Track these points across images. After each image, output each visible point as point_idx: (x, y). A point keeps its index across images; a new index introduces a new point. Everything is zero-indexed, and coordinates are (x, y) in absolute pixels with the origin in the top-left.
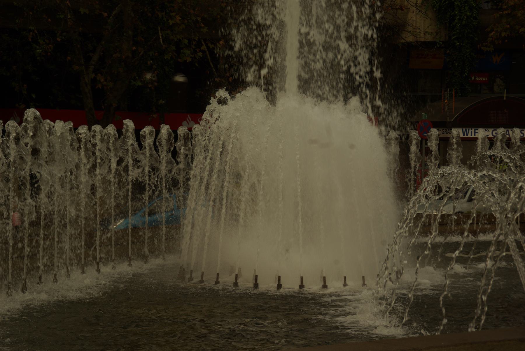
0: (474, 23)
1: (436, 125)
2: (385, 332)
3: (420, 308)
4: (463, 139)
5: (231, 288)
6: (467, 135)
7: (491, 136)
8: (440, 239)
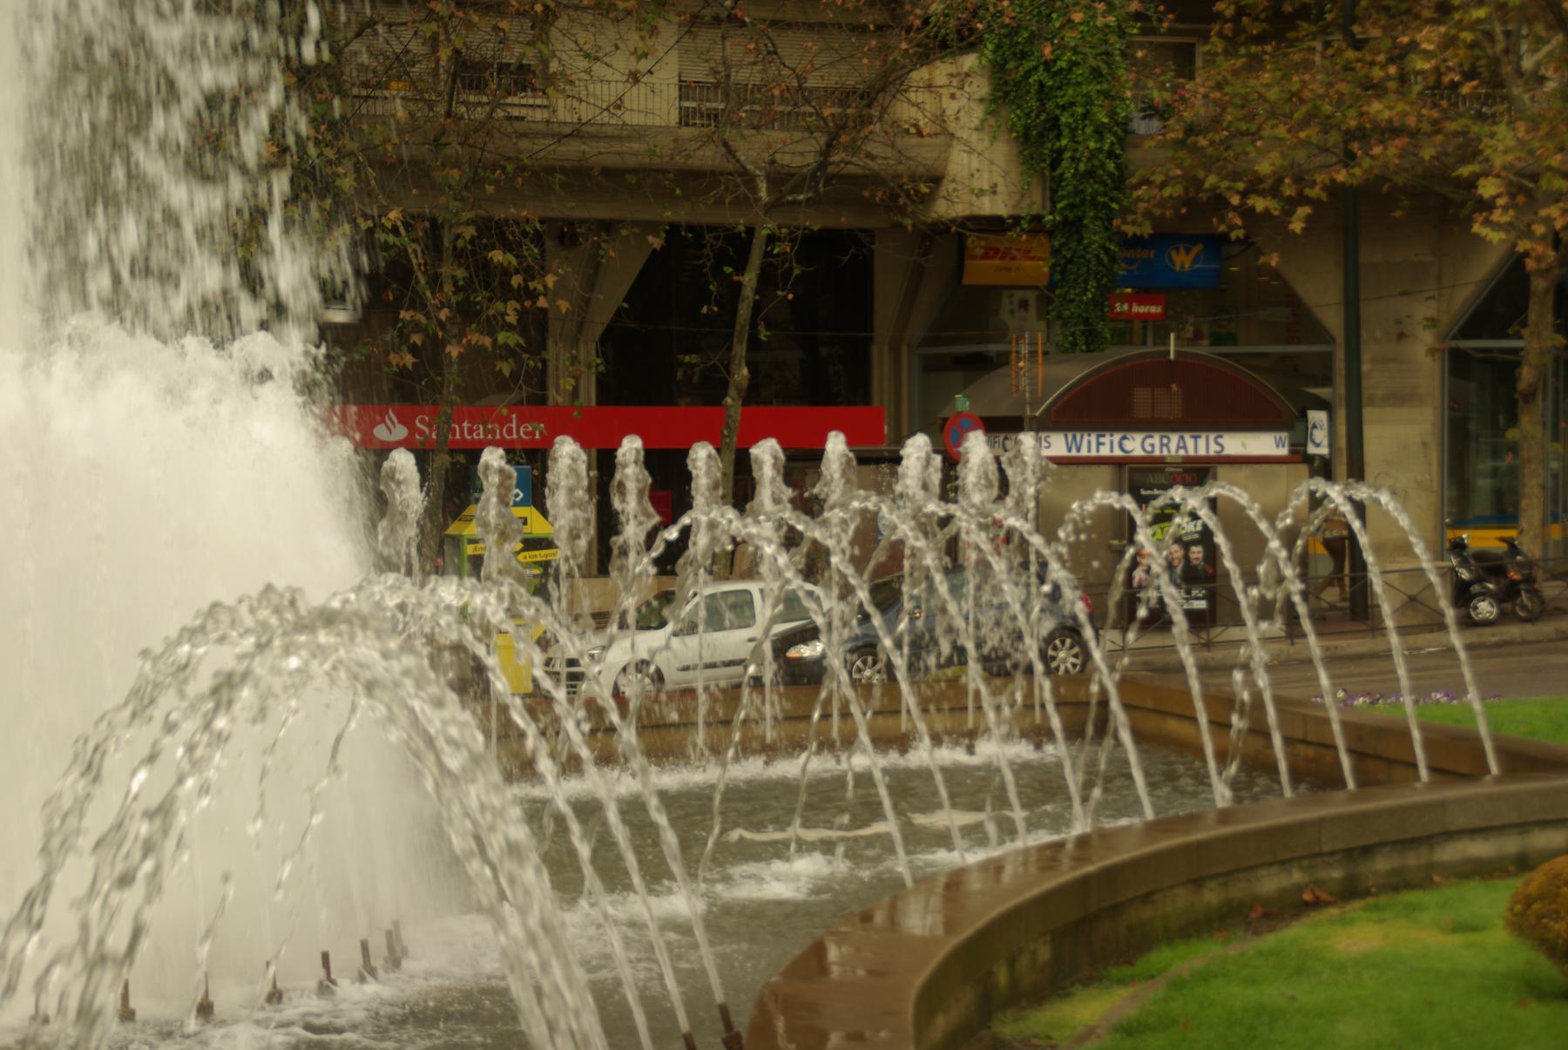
6: (1078, 450)
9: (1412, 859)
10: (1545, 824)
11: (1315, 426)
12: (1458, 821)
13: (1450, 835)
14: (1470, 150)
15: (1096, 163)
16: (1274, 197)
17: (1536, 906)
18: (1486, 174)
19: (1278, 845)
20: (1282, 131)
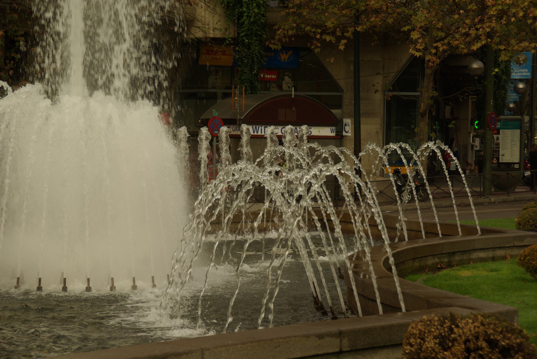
0: (262, 21)
1: (228, 122)
2: (177, 334)
3: (209, 307)
4: (253, 137)
5: (35, 293)
6: (257, 133)
7: (280, 134)
8: (231, 237)
9: (465, 257)
10: (500, 248)
11: (346, 125)
12: (478, 246)
13: (475, 250)
14: (407, 19)
15: (257, 18)
16: (333, 36)
17: (528, 258)
18: (413, 29)
19: (433, 251)
20: (336, 10)
